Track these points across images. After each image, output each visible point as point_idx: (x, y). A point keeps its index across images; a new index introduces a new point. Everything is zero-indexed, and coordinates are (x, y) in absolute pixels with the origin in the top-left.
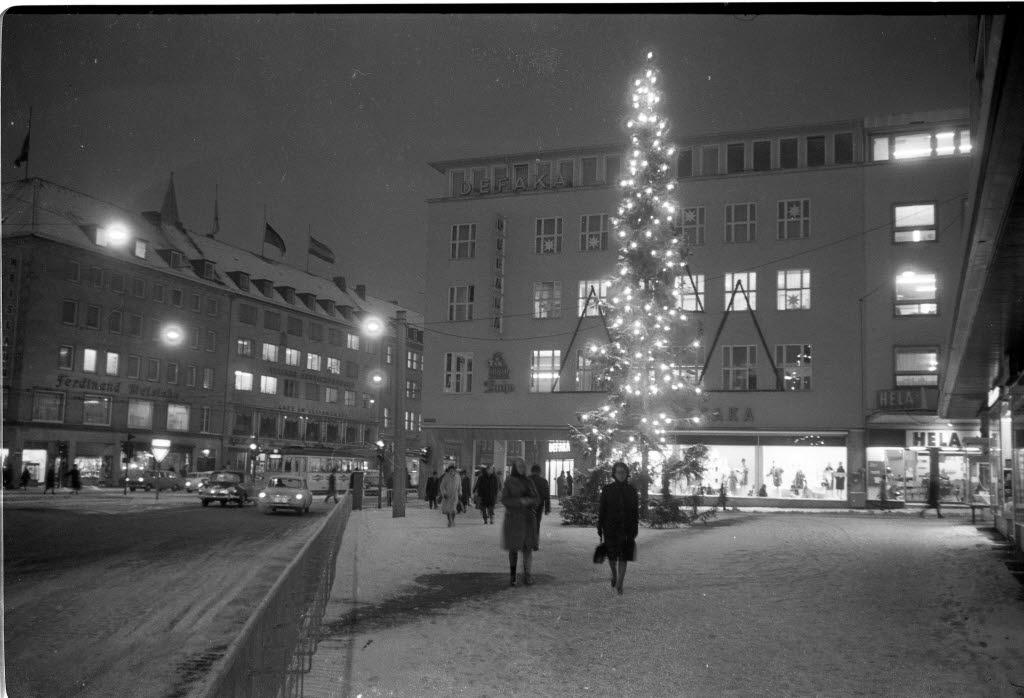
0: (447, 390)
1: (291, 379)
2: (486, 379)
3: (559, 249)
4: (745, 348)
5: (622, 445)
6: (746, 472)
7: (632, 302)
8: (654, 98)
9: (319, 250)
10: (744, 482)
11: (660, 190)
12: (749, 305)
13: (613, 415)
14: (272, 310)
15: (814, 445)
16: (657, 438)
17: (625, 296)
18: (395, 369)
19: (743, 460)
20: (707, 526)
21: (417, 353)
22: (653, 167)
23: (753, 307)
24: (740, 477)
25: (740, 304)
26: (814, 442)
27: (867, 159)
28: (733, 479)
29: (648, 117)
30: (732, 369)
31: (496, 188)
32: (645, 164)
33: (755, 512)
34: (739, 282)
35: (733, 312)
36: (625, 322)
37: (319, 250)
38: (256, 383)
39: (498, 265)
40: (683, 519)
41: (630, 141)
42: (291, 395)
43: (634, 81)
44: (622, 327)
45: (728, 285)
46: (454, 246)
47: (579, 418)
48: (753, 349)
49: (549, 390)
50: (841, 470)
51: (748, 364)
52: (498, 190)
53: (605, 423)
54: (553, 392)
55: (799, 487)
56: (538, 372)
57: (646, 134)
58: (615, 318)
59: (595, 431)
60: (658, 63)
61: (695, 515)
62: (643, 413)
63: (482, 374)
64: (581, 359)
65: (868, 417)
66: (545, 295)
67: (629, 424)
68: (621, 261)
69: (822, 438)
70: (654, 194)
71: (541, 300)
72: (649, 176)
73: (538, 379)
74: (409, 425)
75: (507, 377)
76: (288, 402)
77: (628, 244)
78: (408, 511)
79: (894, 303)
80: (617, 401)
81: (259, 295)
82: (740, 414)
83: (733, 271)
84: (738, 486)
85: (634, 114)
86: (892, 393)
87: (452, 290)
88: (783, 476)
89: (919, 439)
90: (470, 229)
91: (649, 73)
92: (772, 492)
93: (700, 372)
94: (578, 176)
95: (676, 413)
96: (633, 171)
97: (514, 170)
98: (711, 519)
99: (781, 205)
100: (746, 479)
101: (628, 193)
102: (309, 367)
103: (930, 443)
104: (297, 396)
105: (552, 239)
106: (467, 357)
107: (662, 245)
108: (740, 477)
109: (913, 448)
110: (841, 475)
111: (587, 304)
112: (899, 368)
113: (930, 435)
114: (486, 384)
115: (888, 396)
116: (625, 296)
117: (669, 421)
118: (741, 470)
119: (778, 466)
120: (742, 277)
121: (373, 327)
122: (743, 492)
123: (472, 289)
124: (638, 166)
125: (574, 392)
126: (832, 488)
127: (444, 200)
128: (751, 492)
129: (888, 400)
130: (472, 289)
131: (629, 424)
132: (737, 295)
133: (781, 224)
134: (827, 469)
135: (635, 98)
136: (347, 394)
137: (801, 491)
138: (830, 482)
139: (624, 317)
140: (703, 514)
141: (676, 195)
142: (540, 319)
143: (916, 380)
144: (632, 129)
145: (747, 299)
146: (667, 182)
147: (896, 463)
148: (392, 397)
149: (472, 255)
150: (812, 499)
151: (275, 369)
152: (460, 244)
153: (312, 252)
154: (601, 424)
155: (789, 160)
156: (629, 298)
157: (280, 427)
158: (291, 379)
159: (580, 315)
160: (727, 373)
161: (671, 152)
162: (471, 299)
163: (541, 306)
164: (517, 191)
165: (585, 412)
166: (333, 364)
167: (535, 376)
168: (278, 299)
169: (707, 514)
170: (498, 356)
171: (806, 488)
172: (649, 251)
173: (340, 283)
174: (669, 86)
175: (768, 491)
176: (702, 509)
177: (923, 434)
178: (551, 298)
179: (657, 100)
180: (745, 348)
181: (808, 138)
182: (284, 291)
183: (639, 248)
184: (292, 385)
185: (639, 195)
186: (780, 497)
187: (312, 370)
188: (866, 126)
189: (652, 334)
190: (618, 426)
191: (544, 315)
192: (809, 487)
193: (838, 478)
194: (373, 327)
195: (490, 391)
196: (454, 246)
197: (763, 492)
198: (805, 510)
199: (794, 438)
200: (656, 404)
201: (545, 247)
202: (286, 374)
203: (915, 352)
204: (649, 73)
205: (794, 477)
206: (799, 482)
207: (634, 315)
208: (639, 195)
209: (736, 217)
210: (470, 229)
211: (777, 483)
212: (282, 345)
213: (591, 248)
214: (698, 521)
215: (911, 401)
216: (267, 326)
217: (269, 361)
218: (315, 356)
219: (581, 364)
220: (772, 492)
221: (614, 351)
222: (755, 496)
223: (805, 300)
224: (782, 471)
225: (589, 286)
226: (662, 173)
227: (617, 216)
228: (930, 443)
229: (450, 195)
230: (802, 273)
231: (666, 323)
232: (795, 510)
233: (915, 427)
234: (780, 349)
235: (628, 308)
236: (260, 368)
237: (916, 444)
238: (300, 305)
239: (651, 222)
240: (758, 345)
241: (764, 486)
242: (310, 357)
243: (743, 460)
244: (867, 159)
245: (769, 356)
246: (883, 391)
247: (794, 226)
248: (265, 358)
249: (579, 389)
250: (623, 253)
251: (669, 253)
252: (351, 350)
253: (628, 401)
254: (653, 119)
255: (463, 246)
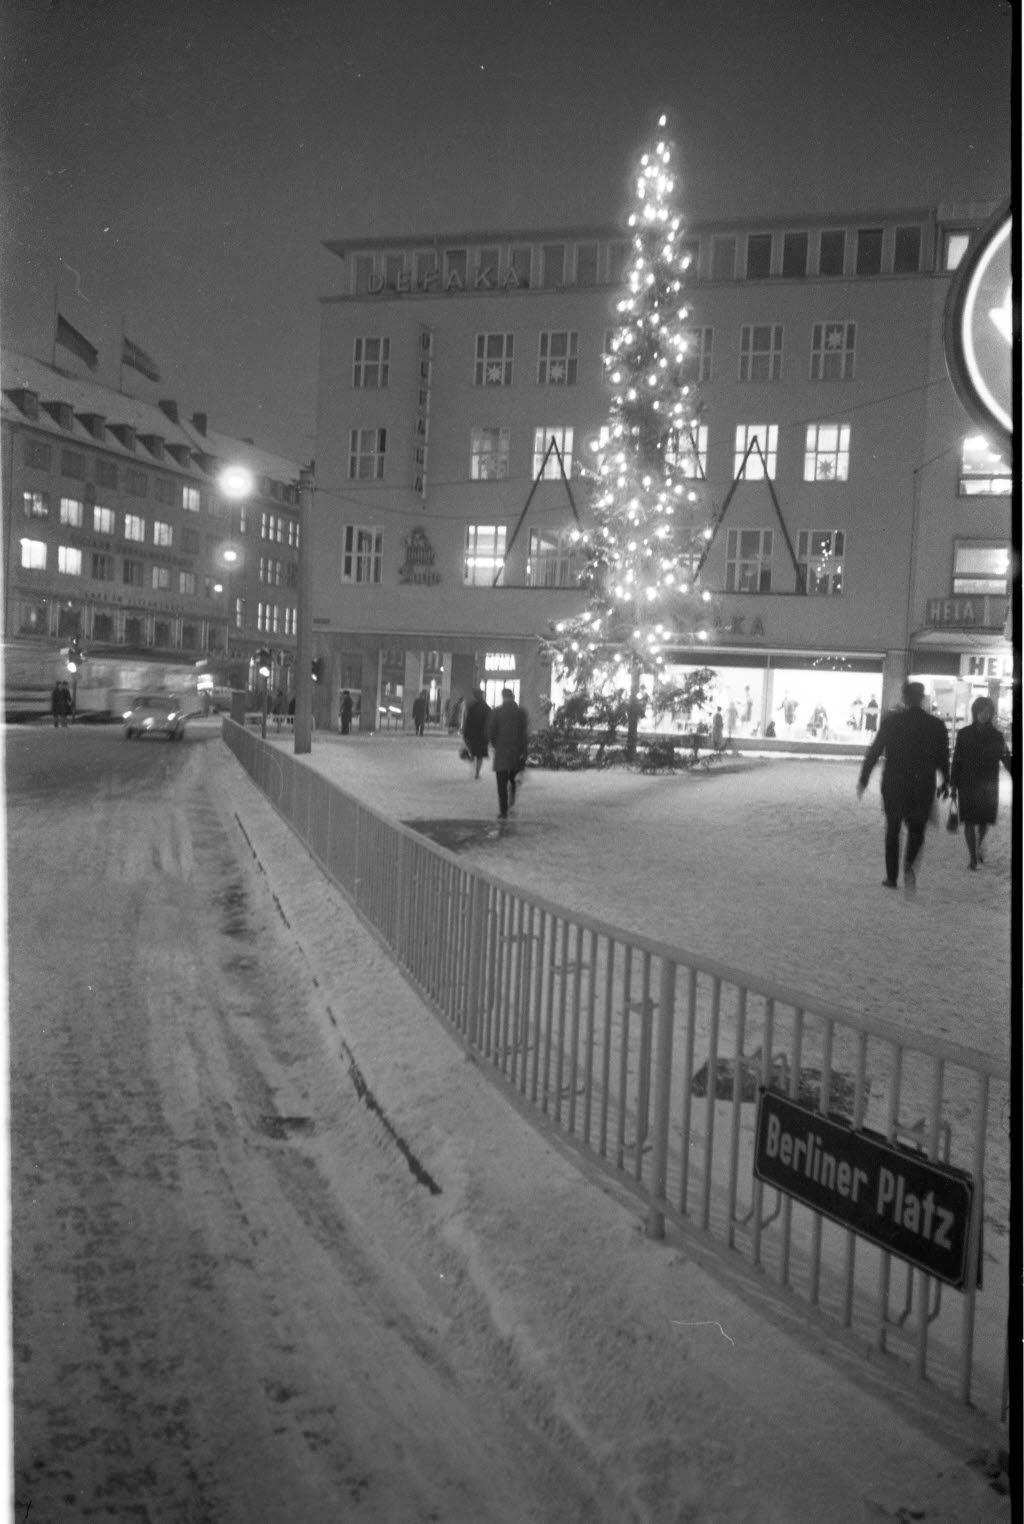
0: (345, 579)
1: (100, 550)
2: (401, 563)
3: (508, 381)
4: (758, 533)
5: (606, 665)
6: (750, 705)
7: (627, 474)
8: (665, 185)
9: (135, 358)
10: (747, 718)
11: (669, 318)
12: (766, 472)
13: (596, 626)
14: (73, 448)
15: (837, 669)
16: (652, 658)
17: (618, 466)
18: (257, 548)
19: (747, 688)
20: (709, 773)
21: (283, 518)
22: (661, 285)
23: (772, 475)
24: (742, 711)
25: (754, 472)
26: (827, 665)
27: (938, 268)
28: (733, 712)
29: (657, 210)
30: (738, 562)
31: (420, 284)
32: (651, 279)
33: (761, 757)
34: (755, 439)
35: (744, 481)
36: (617, 500)
37: (135, 358)
38: (52, 557)
39: (422, 401)
40: (682, 763)
41: (630, 246)
42: (102, 577)
43: (639, 158)
44: (611, 508)
45: (740, 443)
46: (358, 369)
47: (553, 629)
48: (768, 535)
49: (491, 584)
50: (873, 704)
51: (760, 555)
52: (422, 289)
53: (585, 636)
54: (494, 586)
55: (818, 726)
56: (475, 556)
57: (654, 236)
58: (602, 495)
59: (575, 646)
60: (673, 133)
61: (695, 760)
62: (635, 623)
63: (394, 557)
64: (534, 541)
65: (913, 635)
66: (487, 446)
67: (618, 636)
68: (614, 415)
69: (848, 660)
70: (662, 323)
71: (481, 453)
72: (655, 297)
73: (474, 568)
74: (264, 624)
75: (431, 562)
76: (98, 587)
77: (624, 394)
78: (314, 746)
79: (960, 478)
80: (602, 607)
81: (54, 427)
82: (747, 626)
83: (748, 423)
84: (738, 723)
85: (638, 206)
86: (947, 604)
87: (355, 434)
88: (796, 712)
89: (976, 666)
90: (382, 344)
91: (661, 147)
92: (783, 733)
93: (696, 565)
94: (537, 277)
95: (680, 626)
96: (635, 287)
97: (445, 258)
98: (716, 765)
99: (818, 330)
100: (749, 713)
101: (627, 320)
102: (127, 535)
103: (991, 673)
104: (111, 578)
105: (498, 364)
106: (374, 531)
107: (669, 396)
108: (742, 711)
109: (968, 678)
110: (873, 711)
111: (545, 461)
112: (958, 570)
113: (991, 661)
114: (401, 572)
115: (942, 606)
116: (618, 466)
117: (667, 636)
118: (744, 701)
119: (791, 698)
120: (758, 430)
121: (236, 482)
122: (743, 731)
123: (383, 434)
124: (641, 280)
125: (524, 588)
126: (861, 728)
127: (344, 298)
128: (755, 731)
129: (942, 611)
130: (383, 434)
131: (618, 636)
132: (751, 457)
133: (816, 358)
134: (855, 703)
135: (641, 184)
136: (182, 576)
137: (819, 731)
138: (858, 722)
139: (615, 494)
140: (704, 757)
141: (693, 326)
142: (480, 481)
143: (978, 586)
144: (636, 229)
145: (764, 463)
146: (679, 307)
147: (945, 697)
148: (245, 584)
149: (384, 383)
150: (838, 742)
151: (79, 537)
152: (366, 367)
153: (126, 360)
154: (582, 638)
155: (831, 264)
156: (624, 468)
157: (87, 624)
158: (100, 550)
159: (535, 477)
160: (732, 567)
161: (685, 263)
162: (382, 448)
163: (481, 463)
164: (450, 291)
165: (561, 618)
166: (162, 533)
167: (470, 562)
168: (81, 432)
169: (711, 757)
170: (419, 532)
171: (826, 728)
172: (651, 402)
173: (169, 409)
174: (685, 167)
175: (777, 729)
176: (703, 752)
177: (982, 660)
178: (495, 450)
179: (670, 187)
180: (758, 533)
181: (860, 232)
182: (89, 421)
183: (639, 400)
184: (103, 562)
185: (640, 323)
186: (792, 738)
187: (132, 541)
188: (940, 217)
189: (651, 520)
190: (604, 641)
191: (484, 475)
192: (831, 727)
193: (869, 716)
194: (236, 482)
195: (407, 581)
196: (358, 369)
197: (770, 732)
198: (826, 757)
199: (811, 660)
200: (653, 616)
201: (488, 377)
202: (95, 545)
203: (979, 547)
204: (661, 147)
205: (812, 713)
206: (817, 722)
207: (629, 493)
208: (640, 323)
209: (755, 344)
210: (382, 344)
211: (789, 718)
212: (88, 503)
213: (552, 381)
214: (698, 766)
215: (971, 615)
216: (66, 473)
217: (68, 525)
218: (136, 519)
219: (534, 547)
220: (783, 733)
221: (599, 539)
222: (760, 736)
223: (841, 469)
224: (796, 705)
225: (549, 436)
226: (672, 293)
227: (609, 352)
228: (991, 673)
229: (352, 291)
230: (839, 429)
231: (670, 503)
232: (813, 756)
233: (970, 650)
234: (804, 536)
235: (622, 482)
236: (55, 534)
237: (972, 672)
238: (113, 443)
239: (656, 362)
240: (774, 529)
241: (772, 725)
242: (128, 520)
243: (747, 688)
244: (938, 268)
245: (790, 548)
246: (936, 600)
247: (832, 360)
248: (64, 520)
249: (533, 583)
250: (615, 404)
251: (678, 408)
252: (188, 510)
253: (617, 608)
254: (663, 215)
255: (371, 370)
